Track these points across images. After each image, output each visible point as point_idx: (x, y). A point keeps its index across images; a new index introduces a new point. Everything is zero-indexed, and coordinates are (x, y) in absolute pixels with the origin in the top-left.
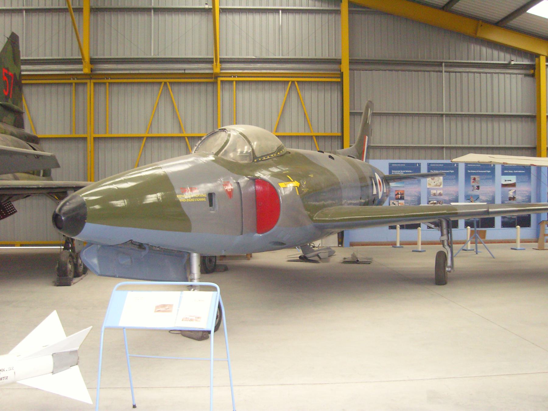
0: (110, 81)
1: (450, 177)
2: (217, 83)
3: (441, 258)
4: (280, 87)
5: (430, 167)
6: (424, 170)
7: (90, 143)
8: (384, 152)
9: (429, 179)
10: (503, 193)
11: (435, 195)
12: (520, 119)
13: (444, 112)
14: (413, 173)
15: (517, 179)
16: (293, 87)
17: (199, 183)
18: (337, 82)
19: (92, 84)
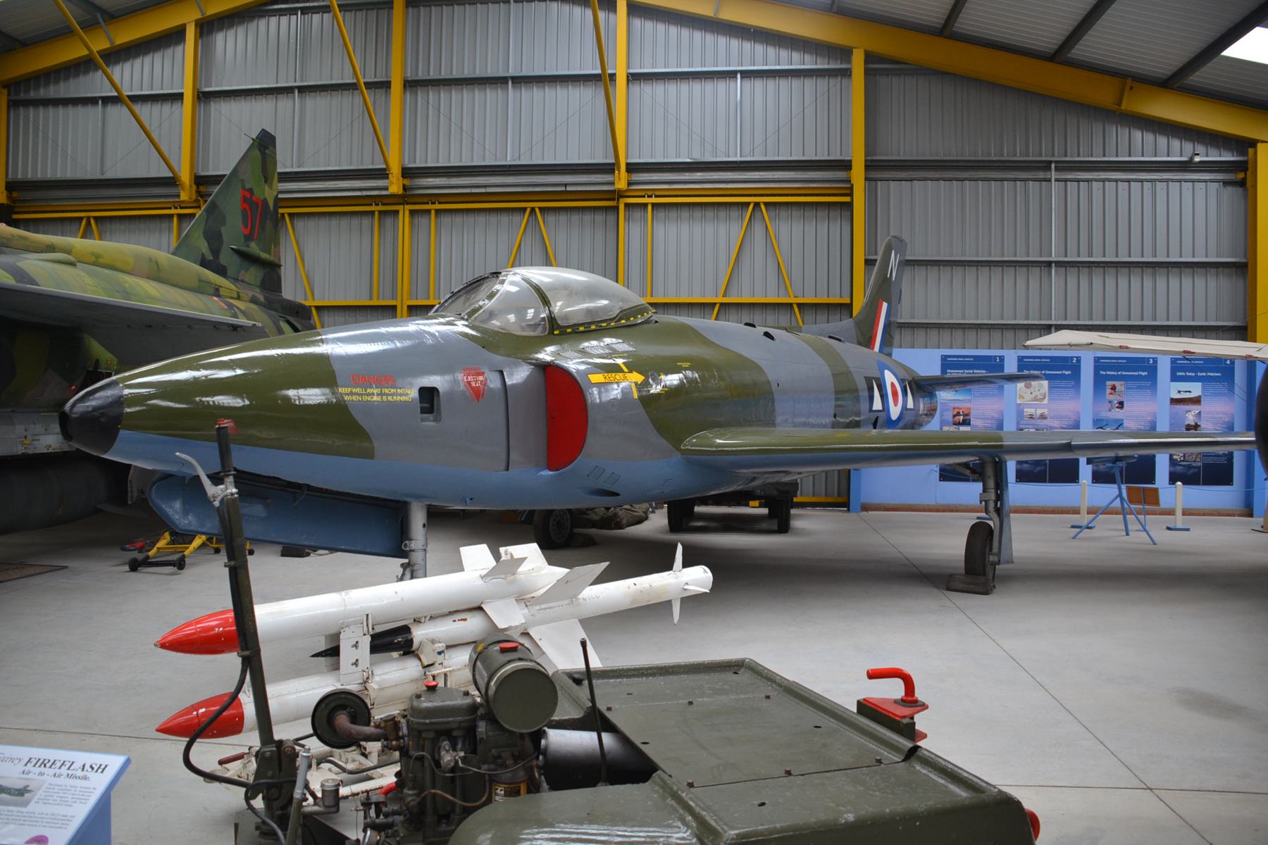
0: (437, 206)
1: (1063, 383)
2: (617, 208)
4: (735, 213)
6: (1011, 367)
10: (1173, 416)
11: (1031, 417)
12: (1213, 270)
13: (1053, 258)
14: (987, 374)
15: (1203, 389)
16: (758, 214)
18: (842, 204)
19: (407, 213)
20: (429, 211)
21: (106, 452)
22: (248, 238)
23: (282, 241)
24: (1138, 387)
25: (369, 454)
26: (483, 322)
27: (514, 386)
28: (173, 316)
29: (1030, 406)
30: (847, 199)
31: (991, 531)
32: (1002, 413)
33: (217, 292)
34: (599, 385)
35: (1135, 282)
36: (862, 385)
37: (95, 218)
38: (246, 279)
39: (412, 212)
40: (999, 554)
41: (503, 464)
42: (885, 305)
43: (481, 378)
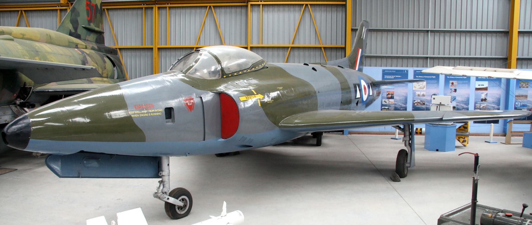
0: (170, 5)
1: (432, 82)
2: (247, 6)
3: (402, 154)
4: (297, 8)
5: (416, 73)
6: (411, 77)
7: (155, 51)
8: (379, 60)
9: (415, 84)
10: (476, 95)
11: (419, 95)
12: (495, 34)
13: (430, 29)
14: (401, 78)
15: (489, 85)
16: (307, 9)
17: (80, 117)
18: (342, 5)
19: (157, 9)
20: (166, 7)
21: (25, 147)
22: (90, 21)
23: (104, 22)
24: (463, 83)
25: (142, 138)
26: (192, 74)
27: (206, 102)
28: (56, 66)
29: (418, 91)
30: (344, 3)
31: (407, 154)
32: (407, 94)
33: (77, 46)
34: (244, 101)
35: (463, 39)
36: (352, 86)
37: (25, 11)
38: (89, 39)
39: (159, 8)
40: (410, 163)
41: (202, 139)
42: (360, 50)
43: (192, 101)
